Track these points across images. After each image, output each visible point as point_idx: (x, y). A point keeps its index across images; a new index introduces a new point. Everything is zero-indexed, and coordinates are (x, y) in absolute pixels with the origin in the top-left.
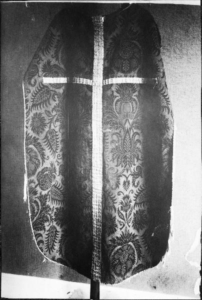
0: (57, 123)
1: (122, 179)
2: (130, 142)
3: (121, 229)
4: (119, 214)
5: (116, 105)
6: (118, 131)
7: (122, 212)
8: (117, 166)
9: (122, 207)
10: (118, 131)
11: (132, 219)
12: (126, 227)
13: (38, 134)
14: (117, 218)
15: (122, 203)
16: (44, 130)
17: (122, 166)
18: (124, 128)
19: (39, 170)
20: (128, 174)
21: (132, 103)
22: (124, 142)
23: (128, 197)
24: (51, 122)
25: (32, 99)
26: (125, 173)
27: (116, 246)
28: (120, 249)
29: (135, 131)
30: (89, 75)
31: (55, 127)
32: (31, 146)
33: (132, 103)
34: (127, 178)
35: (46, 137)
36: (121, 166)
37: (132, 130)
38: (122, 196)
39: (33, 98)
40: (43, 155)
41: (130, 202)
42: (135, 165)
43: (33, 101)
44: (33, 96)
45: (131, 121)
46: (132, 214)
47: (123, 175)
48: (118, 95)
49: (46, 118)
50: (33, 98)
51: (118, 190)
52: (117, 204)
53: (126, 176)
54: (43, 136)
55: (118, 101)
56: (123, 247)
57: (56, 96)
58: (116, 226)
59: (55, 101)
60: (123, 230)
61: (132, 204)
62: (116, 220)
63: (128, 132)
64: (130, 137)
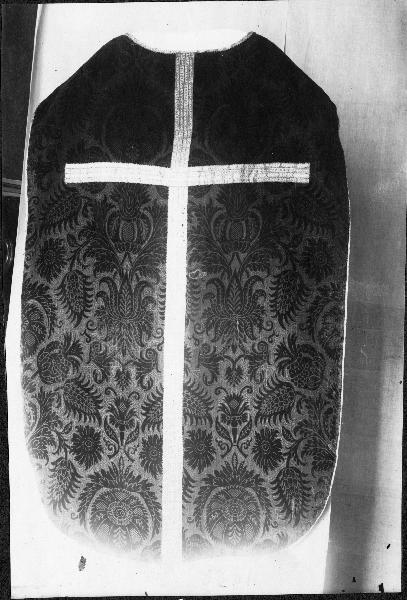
0: (89, 259)
1: (224, 365)
2: (241, 295)
3: (223, 456)
4: (217, 429)
5: (215, 225)
6: (218, 275)
7: (113, 427)
8: (105, 340)
9: (223, 417)
10: (218, 275)
11: (253, 444)
12: (235, 454)
13: (49, 281)
14: (215, 434)
15: (223, 408)
16: (59, 271)
17: (222, 343)
18: (229, 272)
19: (43, 345)
20: (237, 355)
21: (138, 223)
22: (120, 298)
23: (239, 399)
24: (73, 258)
25: (42, 214)
26: (230, 353)
27: (100, 487)
28: (222, 492)
29: (252, 274)
30: (197, 159)
31: (84, 267)
32: (31, 302)
33: (138, 223)
34: (234, 363)
35: (62, 286)
36: (221, 340)
37: (244, 273)
38: (224, 395)
39: (43, 212)
40: (53, 318)
41: (246, 408)
42: (254, 338)
43: (44, 219)
44: (44, 209)
45: (243, 256)
46: (252, 434)
47: (227, 357)
48: (221, 206)
49: (68, 249)
50: (43, 212)
51: (216, 385)
52: (214, 410)
53: (232, 360)
54: (55, 283)
55: (221, 217)
56: (114, 492)
57: (89, 208)
58: (101, 449)
59: (86, 216)
60: (228, 458)
61: (252, 413)
62: (101, 440)
63: (235, 276)
64: (130, 289)
